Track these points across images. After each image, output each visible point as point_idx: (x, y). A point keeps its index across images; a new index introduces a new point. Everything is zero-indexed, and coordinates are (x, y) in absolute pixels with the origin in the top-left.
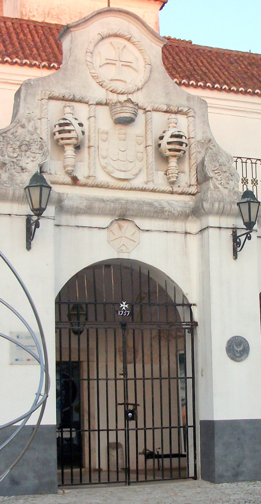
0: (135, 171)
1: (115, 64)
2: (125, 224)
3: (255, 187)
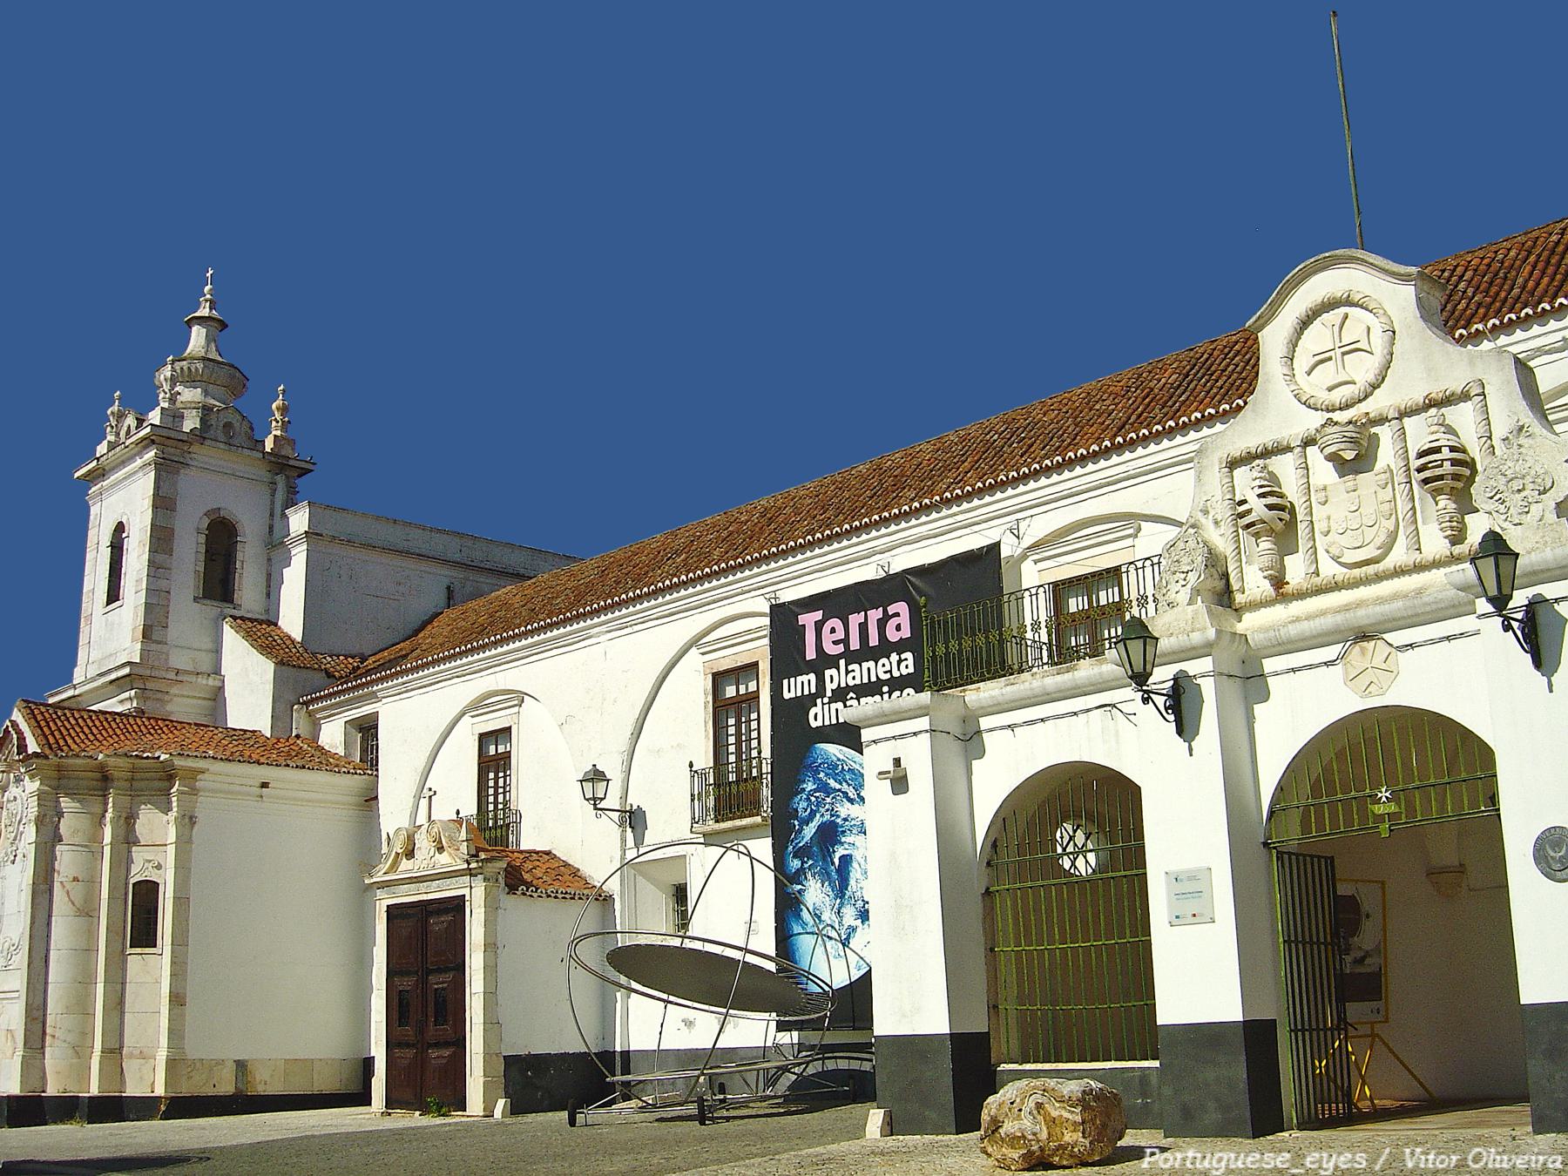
0: (1381, 538)
1: (1330, 359)
3: (1143, 610)
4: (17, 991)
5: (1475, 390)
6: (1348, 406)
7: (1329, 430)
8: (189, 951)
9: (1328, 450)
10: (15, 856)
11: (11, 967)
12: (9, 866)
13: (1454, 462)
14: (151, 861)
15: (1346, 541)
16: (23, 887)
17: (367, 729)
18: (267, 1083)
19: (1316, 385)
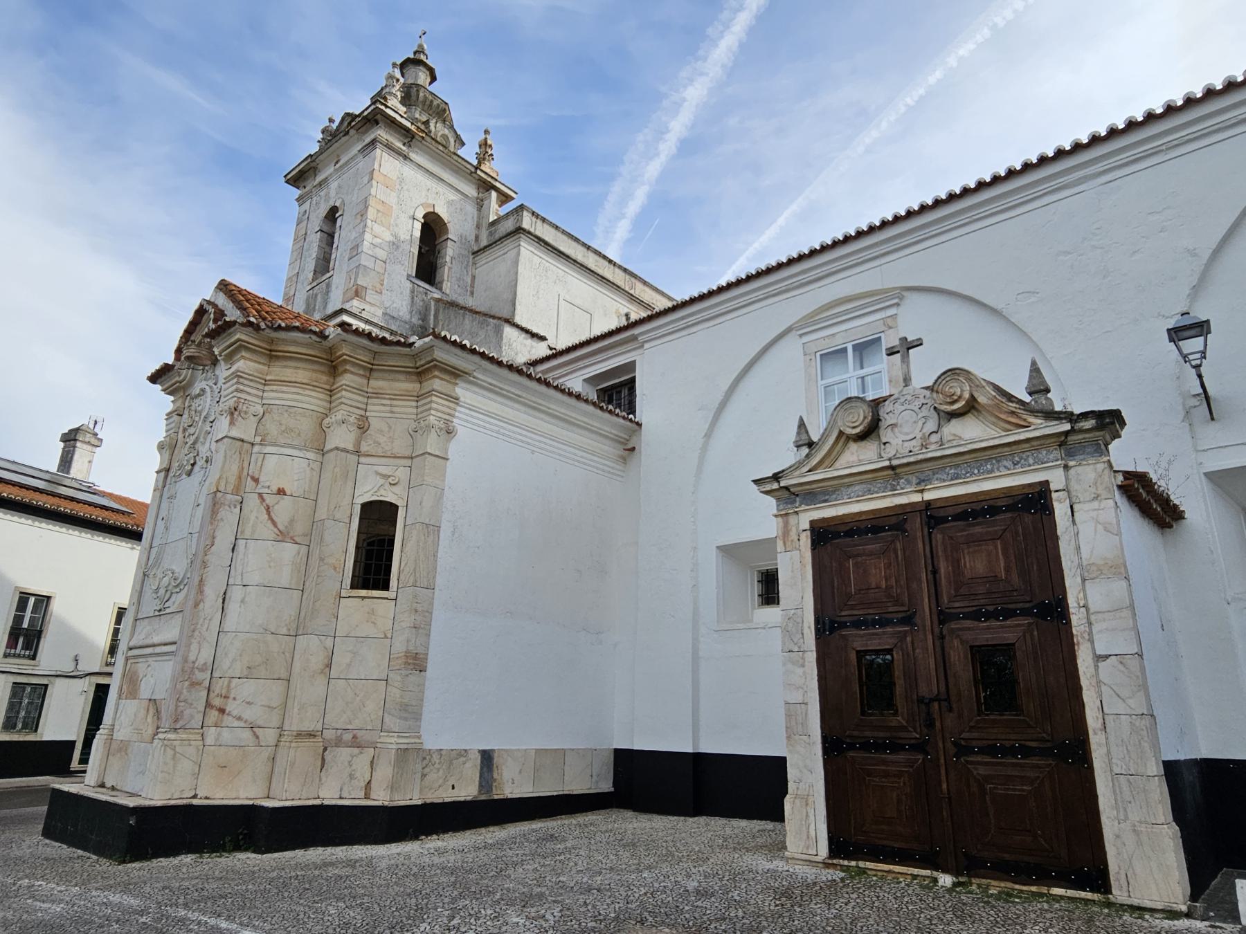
4: (175, 643)
8: (436, 596)
10: (193, 465)
11: (168, 611)
14: (389, 476)
16: (202, 501)
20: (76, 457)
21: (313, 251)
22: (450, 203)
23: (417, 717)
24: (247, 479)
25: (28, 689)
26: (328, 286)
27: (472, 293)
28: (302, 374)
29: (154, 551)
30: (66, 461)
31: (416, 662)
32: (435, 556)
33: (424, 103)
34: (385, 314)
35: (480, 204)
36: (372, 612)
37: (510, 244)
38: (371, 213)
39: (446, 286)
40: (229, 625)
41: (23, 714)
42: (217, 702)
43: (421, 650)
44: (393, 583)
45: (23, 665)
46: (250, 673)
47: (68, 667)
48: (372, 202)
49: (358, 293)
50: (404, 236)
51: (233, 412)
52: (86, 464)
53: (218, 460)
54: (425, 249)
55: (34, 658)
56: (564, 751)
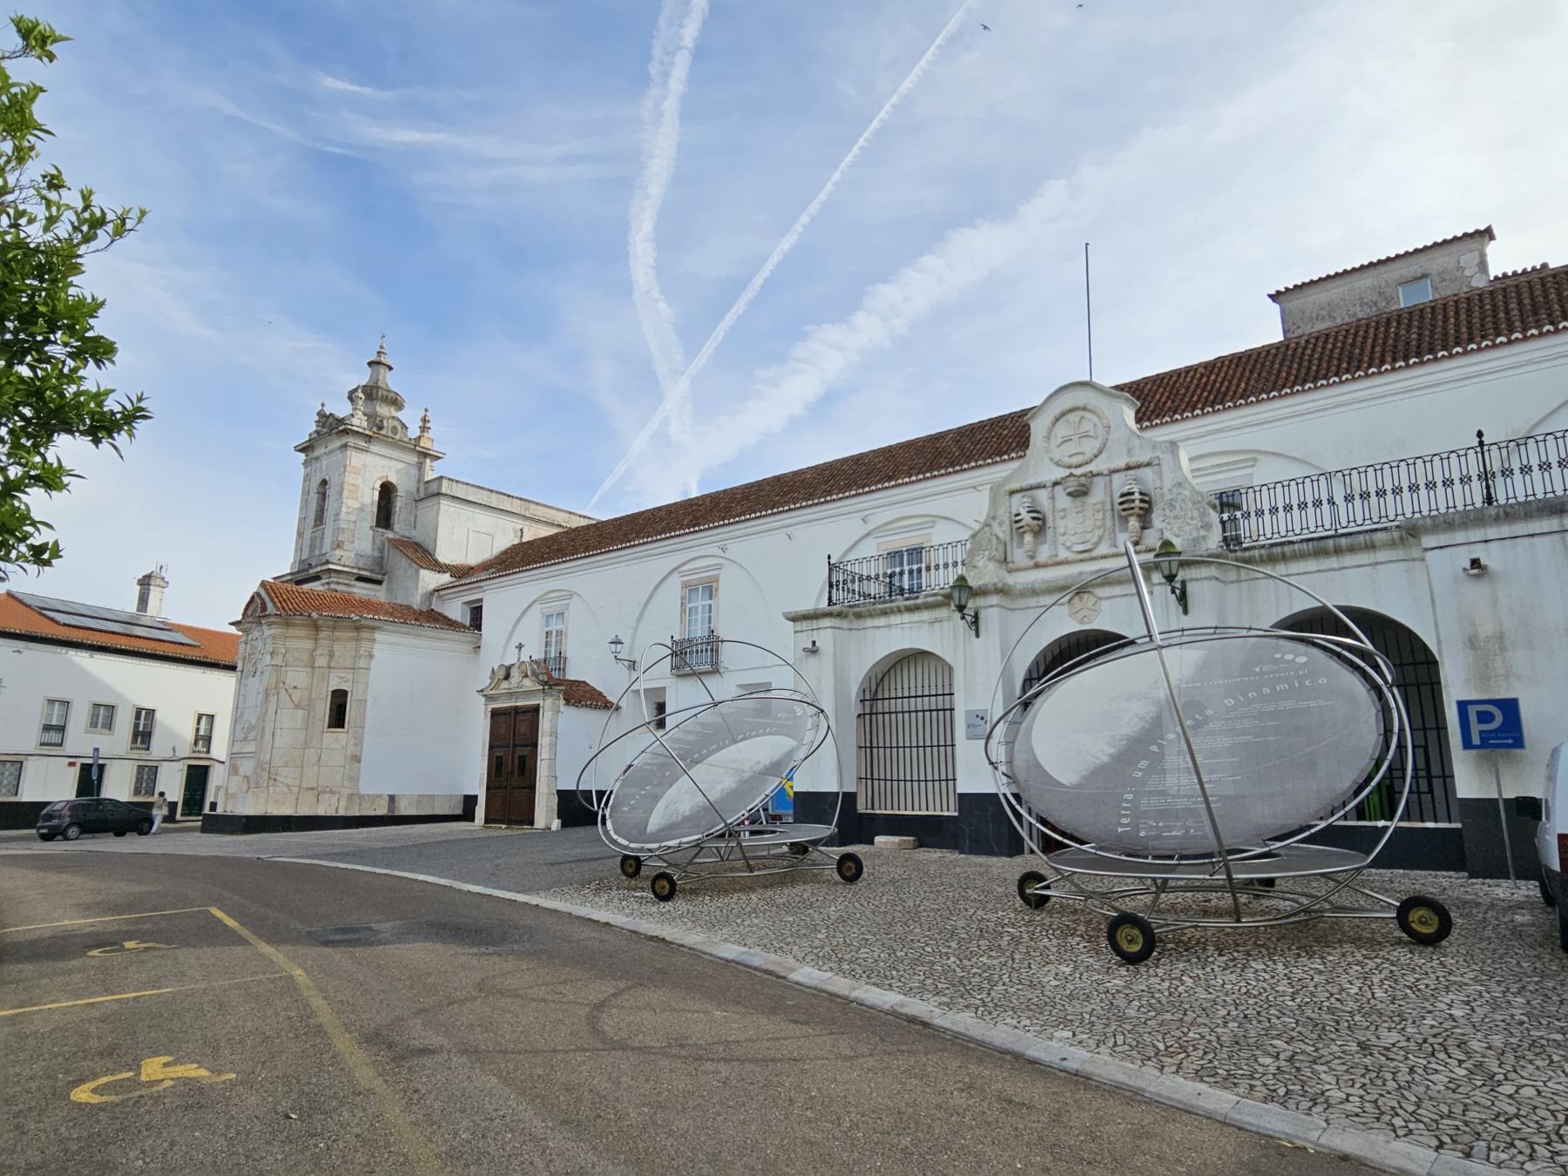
2: (1086, 596)
5: (1156, 462)
6: (1080, 466)
7: (1071, 479)
9: (1069, 490)
12: (251, 679)
13: (1142, 501)
15: (1073, 539)
17: (477, 612)
18: (404, 809)
19: (1063, 453)
20: (151, 598)
21: (313, 507)
22: (398, 471)
23: (358, 781)
24: (280, 683)
25: (146, 769)
26: (323, 534)
27: (415, 527)
28: (303, 633)
29: (239, 710)
30: (143, 602)
31: (357, 759)
32: (365, 713)
33: (382, 398)
34: (356, 555)
35: (420, 466)
36: (337, 738)
37: (434, 500)
38: (346, 493)
39: (397, 527)
40: (276, 745)
41: (144, 785)
42: (273, 776)
43: (358, 754)
44: (346, 725)
45: (143, 754)
46: (286, 764)
47: (169, 755)
48: (346, 486)
49: (339, 546)
50: (368, 501)
51: (272, 654)
52: (158, 602)
53: (267, 674)
54: (383, 503)
55: (148, 749)
56: (433, 796)
